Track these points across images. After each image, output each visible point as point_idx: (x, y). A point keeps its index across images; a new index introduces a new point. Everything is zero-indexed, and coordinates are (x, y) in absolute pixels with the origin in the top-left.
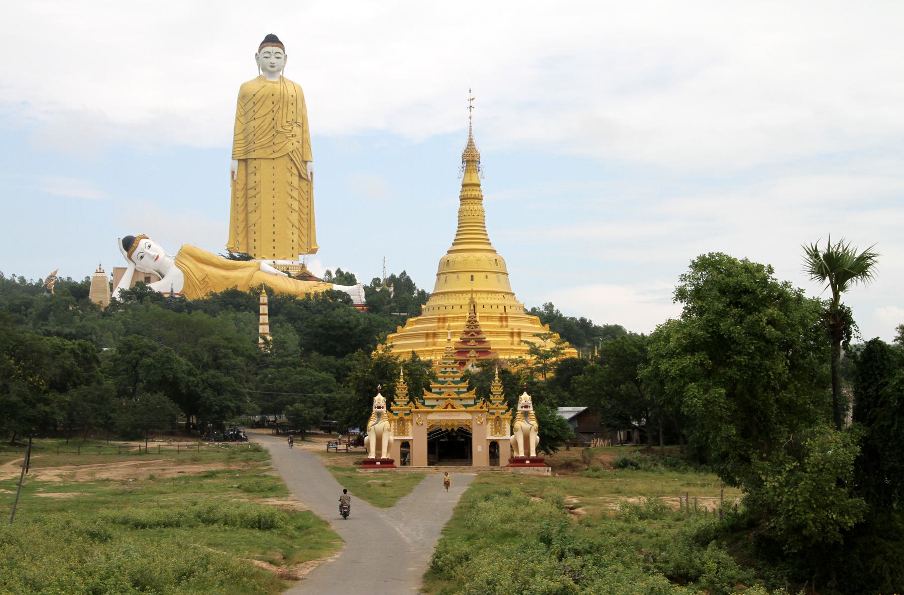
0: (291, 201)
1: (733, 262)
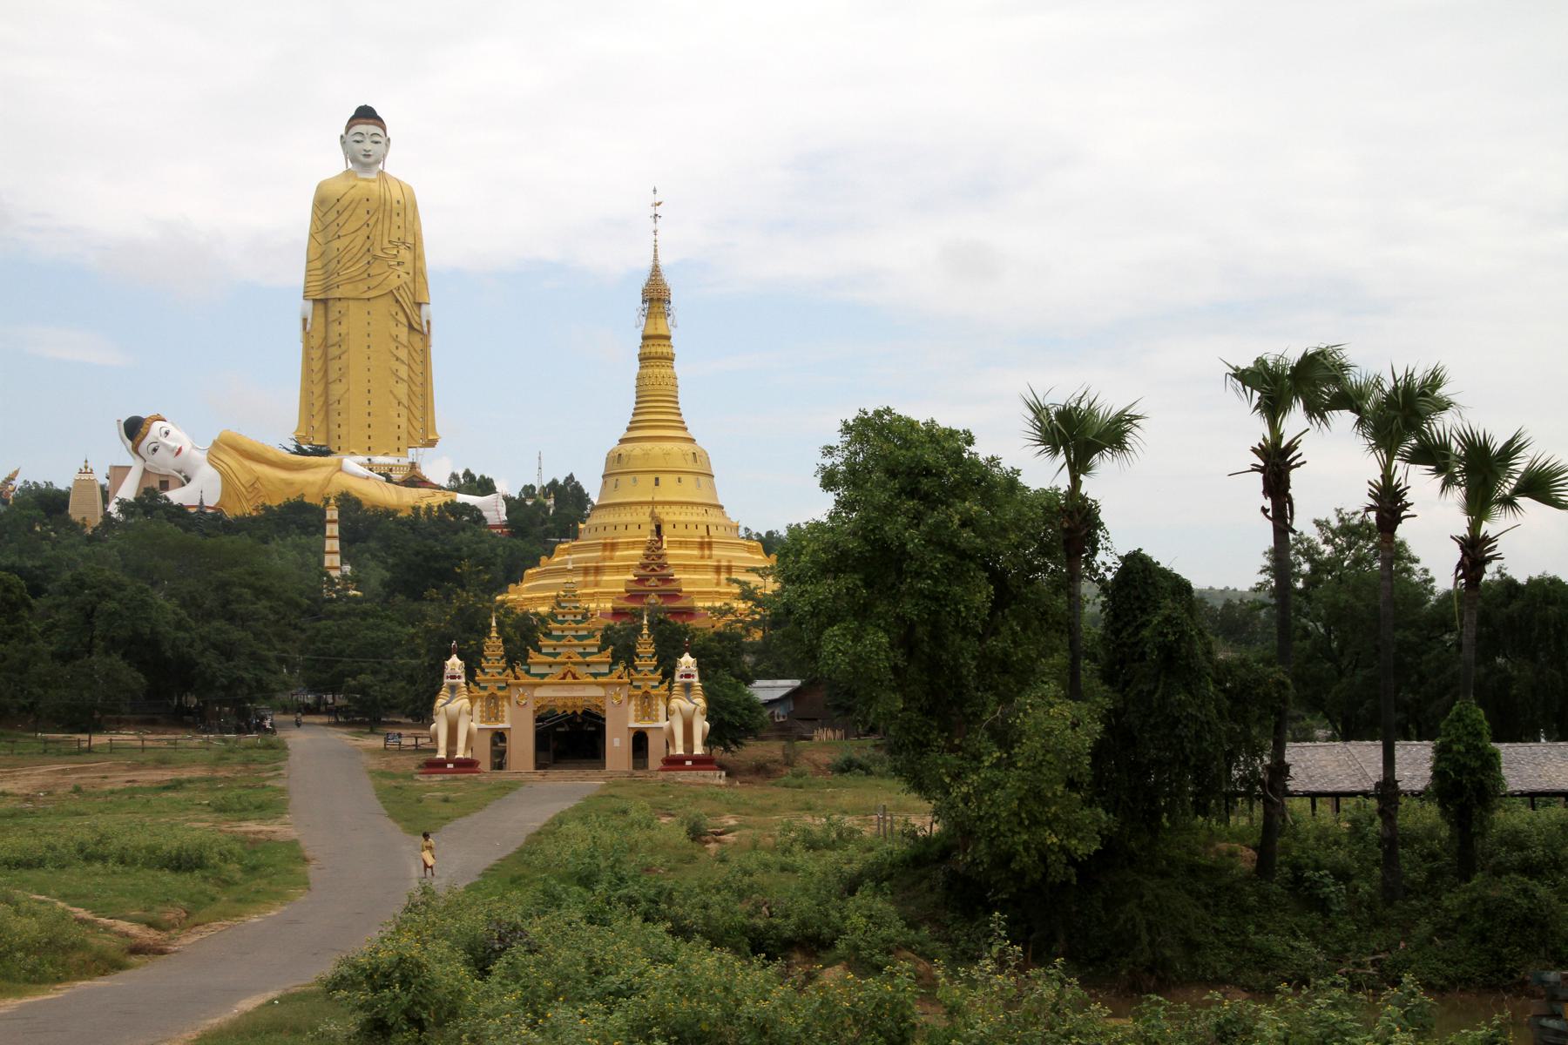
0: (395, 365)
1: (911, 425)
